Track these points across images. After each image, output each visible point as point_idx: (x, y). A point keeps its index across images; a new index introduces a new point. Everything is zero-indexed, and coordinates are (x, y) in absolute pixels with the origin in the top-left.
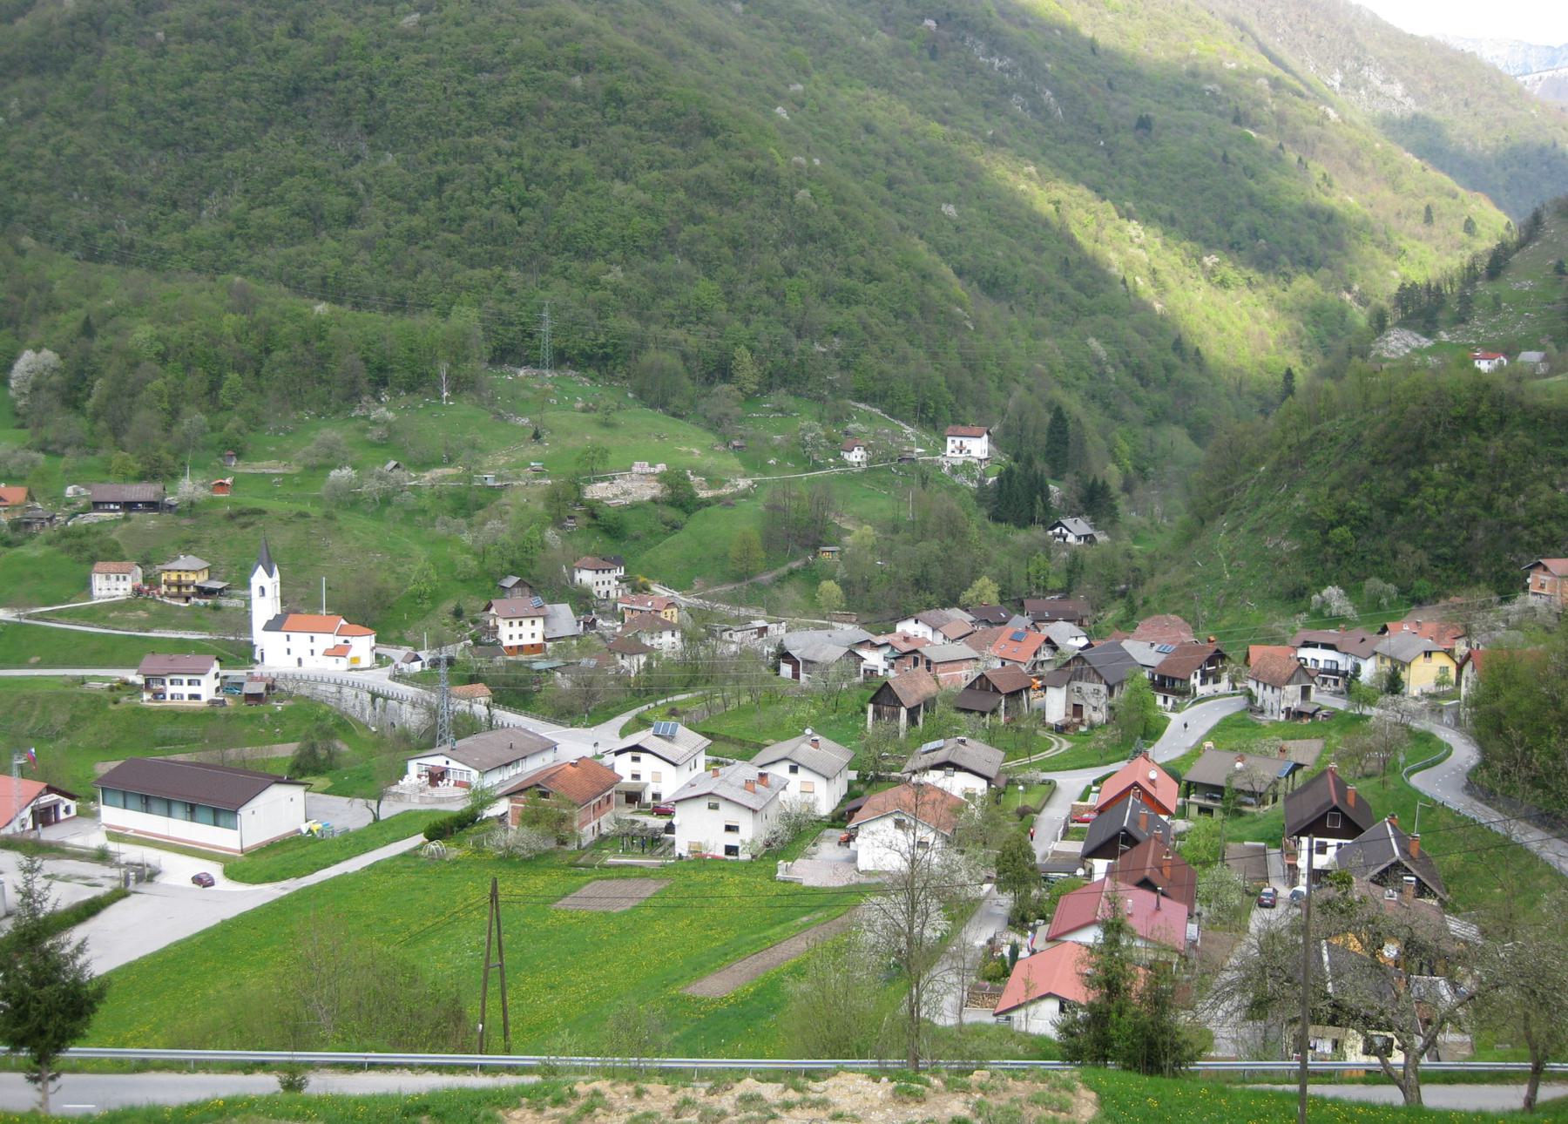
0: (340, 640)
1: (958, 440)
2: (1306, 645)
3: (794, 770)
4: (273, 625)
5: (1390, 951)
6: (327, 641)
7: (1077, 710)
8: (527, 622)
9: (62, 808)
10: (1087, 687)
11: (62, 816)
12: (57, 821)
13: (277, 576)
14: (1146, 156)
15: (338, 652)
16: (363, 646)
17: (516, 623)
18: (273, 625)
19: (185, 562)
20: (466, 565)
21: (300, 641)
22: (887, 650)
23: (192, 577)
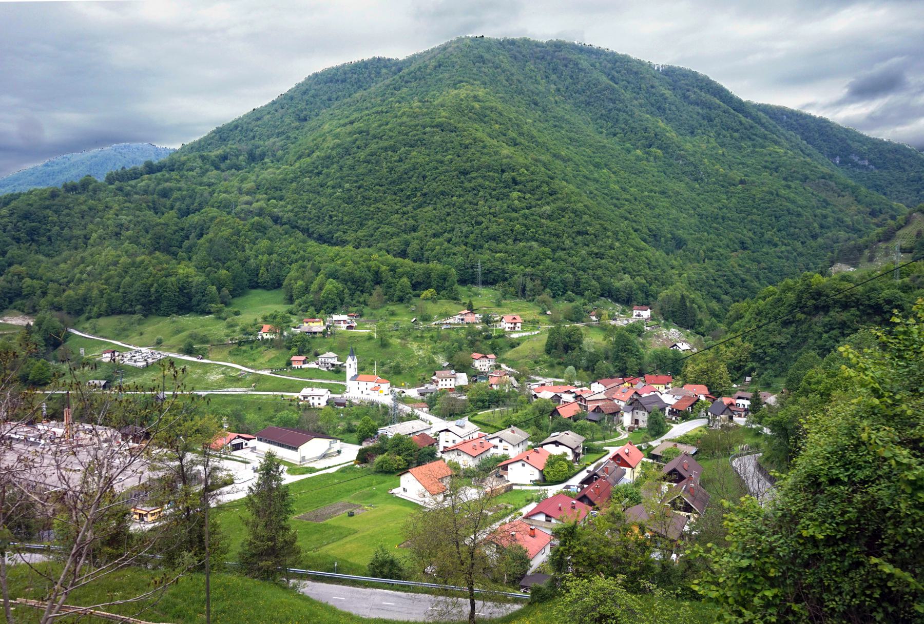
0: (377, 385)
1: (637, 312)
2: (739, 398)
3: (501, 441)
4: (354, 378)
5: (87, 562)
6: (372, 385)
7: (637, 421)
8: (448, 380)
9: (244, 444)
10: (640, 413)
11: (244, 446)
12: (242, 448)
13: (356, 361)
14: (536, 197)
15: (376, 389)
16: (385, 387)
17: (444, 380)
18: (354, 378)
19: (331, 354)
20: (858, 347)
21: (363, 385)
22: (574, 395)
23: (330, 360)
